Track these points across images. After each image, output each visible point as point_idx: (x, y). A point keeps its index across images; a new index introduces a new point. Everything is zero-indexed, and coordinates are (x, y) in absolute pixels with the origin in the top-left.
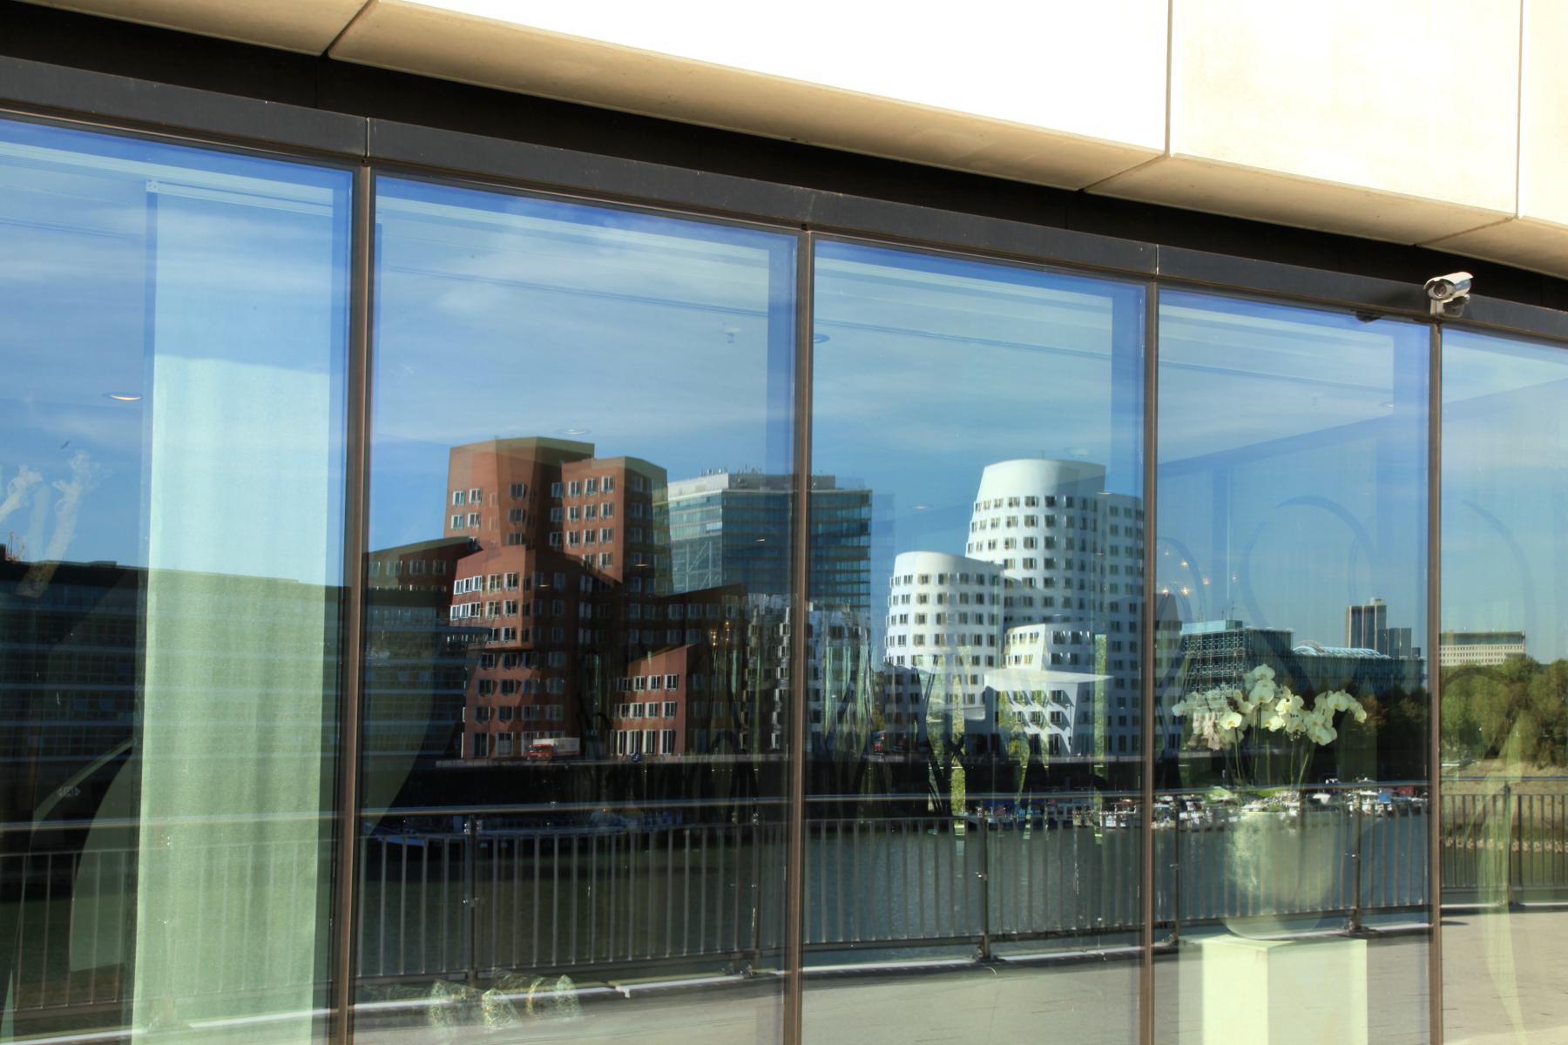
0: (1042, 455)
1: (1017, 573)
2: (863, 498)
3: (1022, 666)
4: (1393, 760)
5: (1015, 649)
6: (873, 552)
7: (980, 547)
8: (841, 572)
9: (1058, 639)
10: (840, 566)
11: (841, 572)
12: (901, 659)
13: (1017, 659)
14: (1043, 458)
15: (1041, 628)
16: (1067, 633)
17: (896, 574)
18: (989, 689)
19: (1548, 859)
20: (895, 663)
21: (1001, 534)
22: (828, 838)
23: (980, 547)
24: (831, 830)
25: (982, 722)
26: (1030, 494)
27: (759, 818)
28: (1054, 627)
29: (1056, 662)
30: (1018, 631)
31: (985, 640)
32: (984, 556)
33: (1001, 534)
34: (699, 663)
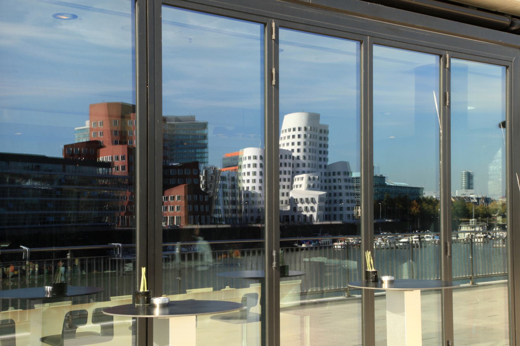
0: (303, 111)
1: (295, 154)
2: (204, 126)
3: (299, 189)
4: (394, 220)
5: (295, 183)
6: (209, 145)
7: (284, 145)
8: (198, 153)
9: (309, 179)
10: (197, 151)
11: (198, 153)
12: (248, 188)
13: (297, 186)
14: (303, 112)
15: (304, 176)
16: (312, 177)
17: (244, 156)
18: (292, 198)
19: (501, 249)
20: (245, 189)
21: (291, 140)
22: (247, 256)
23: (284, 145)
24: (254, 253)
25: (289, 211)
26: (299, 126)
27: (71, 256)
28: (309, 175)
29: (309, 187)
30: (296, 177)
31: (287, 180)
32: (285, 148)
33: (291, 140)
34: (193, 190)
